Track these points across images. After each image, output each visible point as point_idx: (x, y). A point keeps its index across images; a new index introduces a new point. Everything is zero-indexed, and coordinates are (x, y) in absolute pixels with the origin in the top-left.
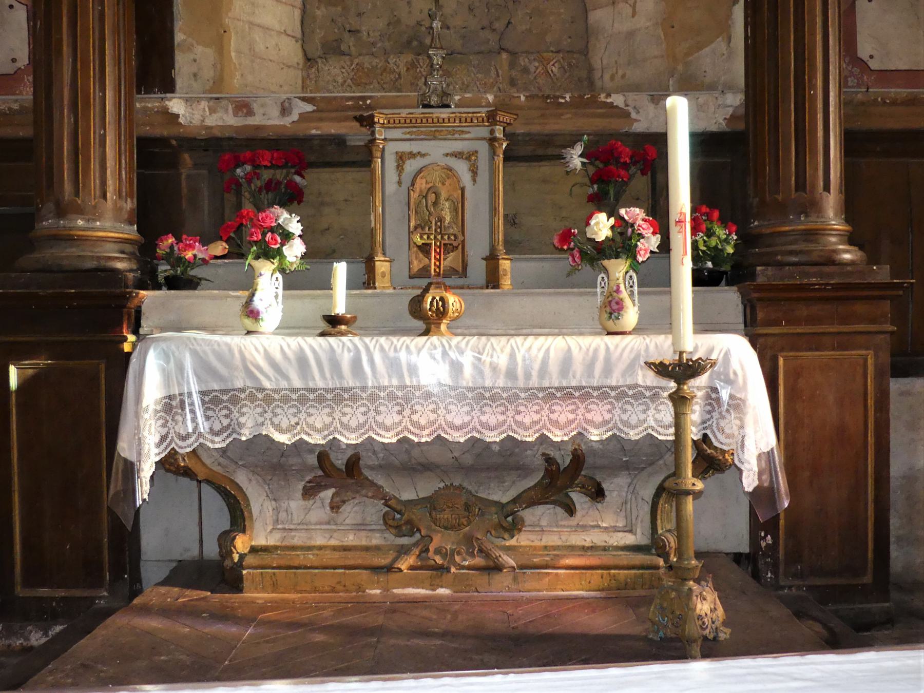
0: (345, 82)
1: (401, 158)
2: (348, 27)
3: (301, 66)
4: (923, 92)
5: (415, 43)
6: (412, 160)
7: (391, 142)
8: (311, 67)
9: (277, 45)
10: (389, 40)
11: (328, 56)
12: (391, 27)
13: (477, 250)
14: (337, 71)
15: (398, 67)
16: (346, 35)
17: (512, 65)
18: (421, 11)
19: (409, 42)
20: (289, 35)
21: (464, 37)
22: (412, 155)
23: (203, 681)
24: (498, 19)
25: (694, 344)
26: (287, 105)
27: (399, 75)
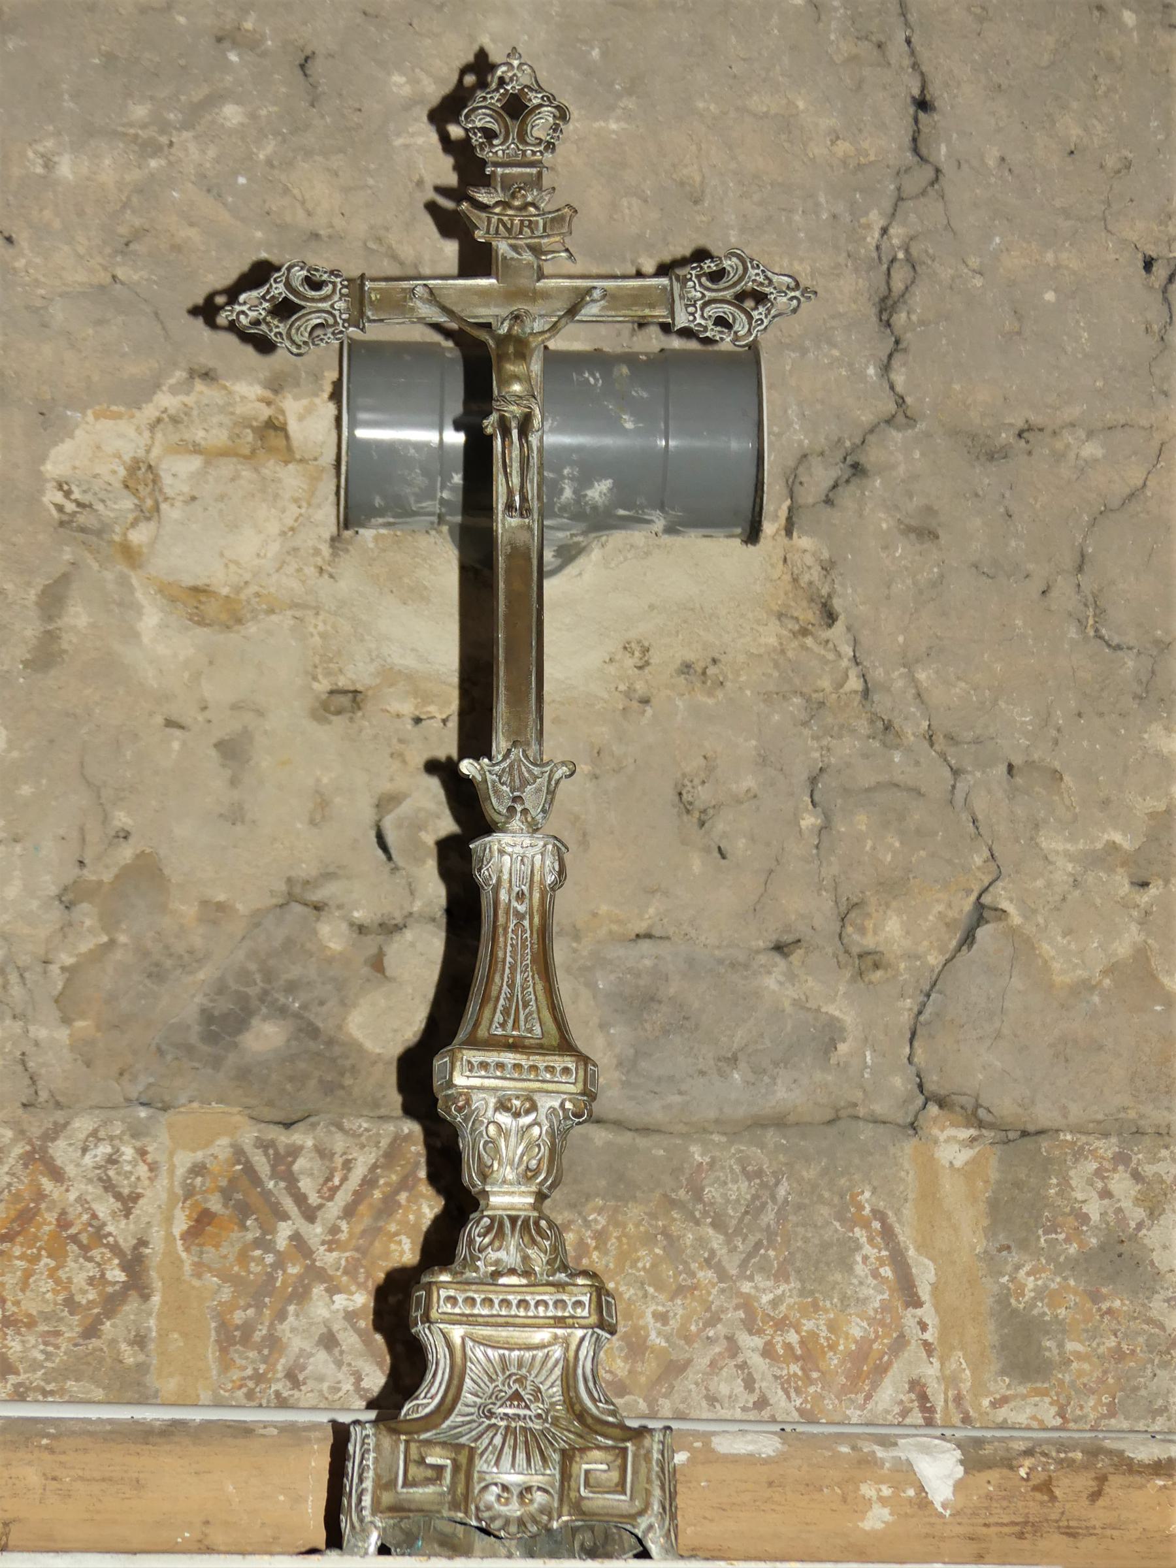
4: (1175, 1451)
5: (266, 1037)
10: (66, 1007)
12: (87, 914)
15: (128, 1202)
17: (1017, 1213)
18: (321, 809)
19: (223, 1025)
23: (867, 1562)
24: (893, 887)
25: (116, 468)
27: (134, 1264)
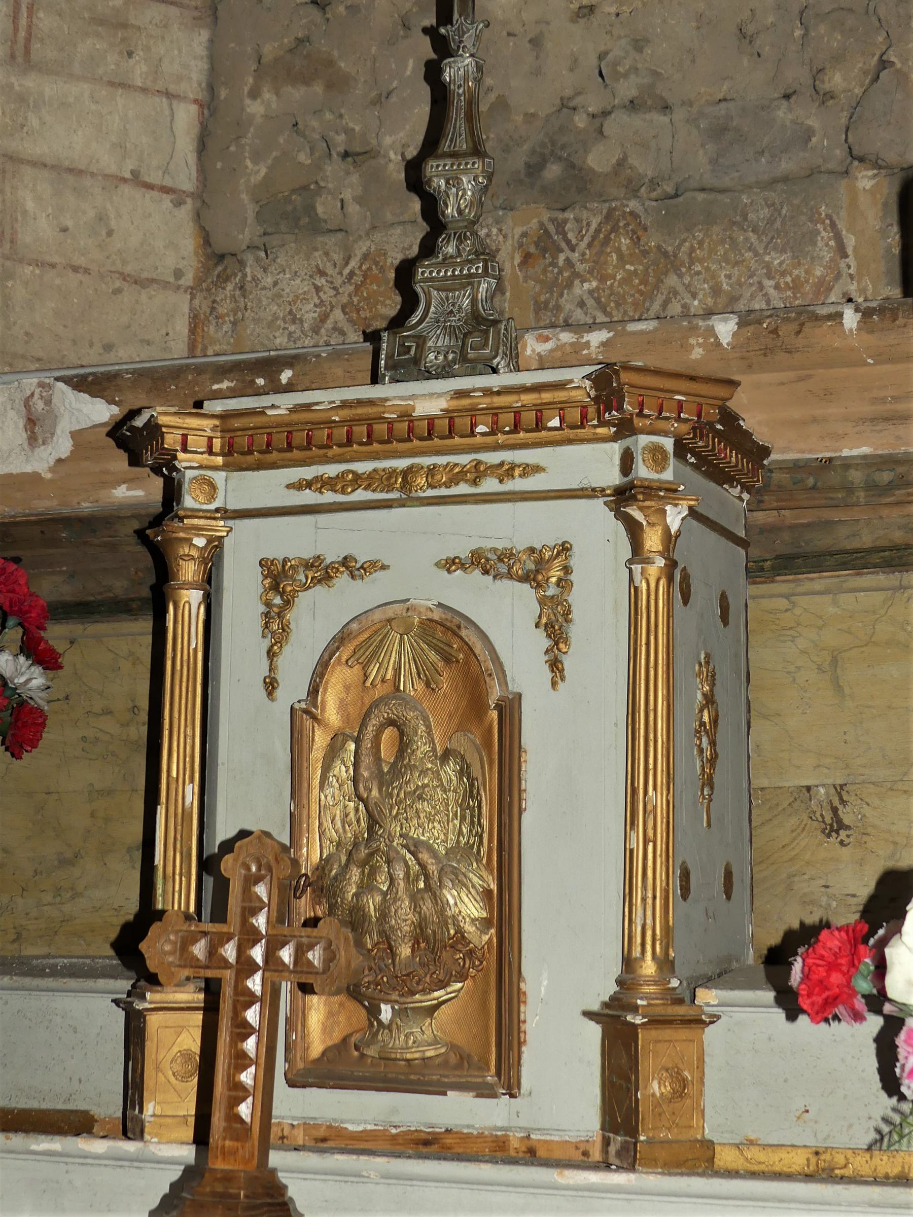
0: (324, 318)
1: (278, 577)
2: (340, 141)
3: (188, 279)
5: (553, 171)
6: (319, 591)
7: (246, 518)
8: (224, 278)
9: (101, 218)
11: (274, 241)
13: (568, 971)
14: (302, 286)
16: (333, 169)
19: (534, 169)
20: (150, 187)
21: (719, 132)
22: (322, 572)
24: (838, 58)
26: (39, 405)
